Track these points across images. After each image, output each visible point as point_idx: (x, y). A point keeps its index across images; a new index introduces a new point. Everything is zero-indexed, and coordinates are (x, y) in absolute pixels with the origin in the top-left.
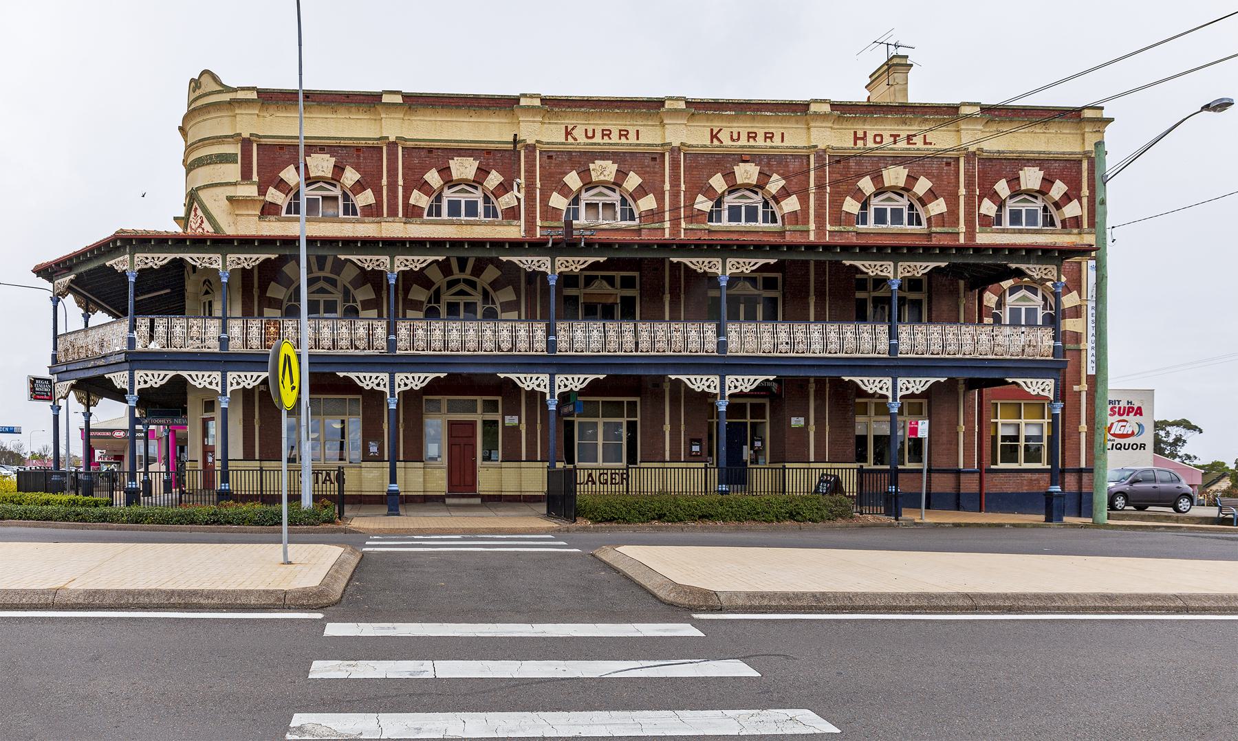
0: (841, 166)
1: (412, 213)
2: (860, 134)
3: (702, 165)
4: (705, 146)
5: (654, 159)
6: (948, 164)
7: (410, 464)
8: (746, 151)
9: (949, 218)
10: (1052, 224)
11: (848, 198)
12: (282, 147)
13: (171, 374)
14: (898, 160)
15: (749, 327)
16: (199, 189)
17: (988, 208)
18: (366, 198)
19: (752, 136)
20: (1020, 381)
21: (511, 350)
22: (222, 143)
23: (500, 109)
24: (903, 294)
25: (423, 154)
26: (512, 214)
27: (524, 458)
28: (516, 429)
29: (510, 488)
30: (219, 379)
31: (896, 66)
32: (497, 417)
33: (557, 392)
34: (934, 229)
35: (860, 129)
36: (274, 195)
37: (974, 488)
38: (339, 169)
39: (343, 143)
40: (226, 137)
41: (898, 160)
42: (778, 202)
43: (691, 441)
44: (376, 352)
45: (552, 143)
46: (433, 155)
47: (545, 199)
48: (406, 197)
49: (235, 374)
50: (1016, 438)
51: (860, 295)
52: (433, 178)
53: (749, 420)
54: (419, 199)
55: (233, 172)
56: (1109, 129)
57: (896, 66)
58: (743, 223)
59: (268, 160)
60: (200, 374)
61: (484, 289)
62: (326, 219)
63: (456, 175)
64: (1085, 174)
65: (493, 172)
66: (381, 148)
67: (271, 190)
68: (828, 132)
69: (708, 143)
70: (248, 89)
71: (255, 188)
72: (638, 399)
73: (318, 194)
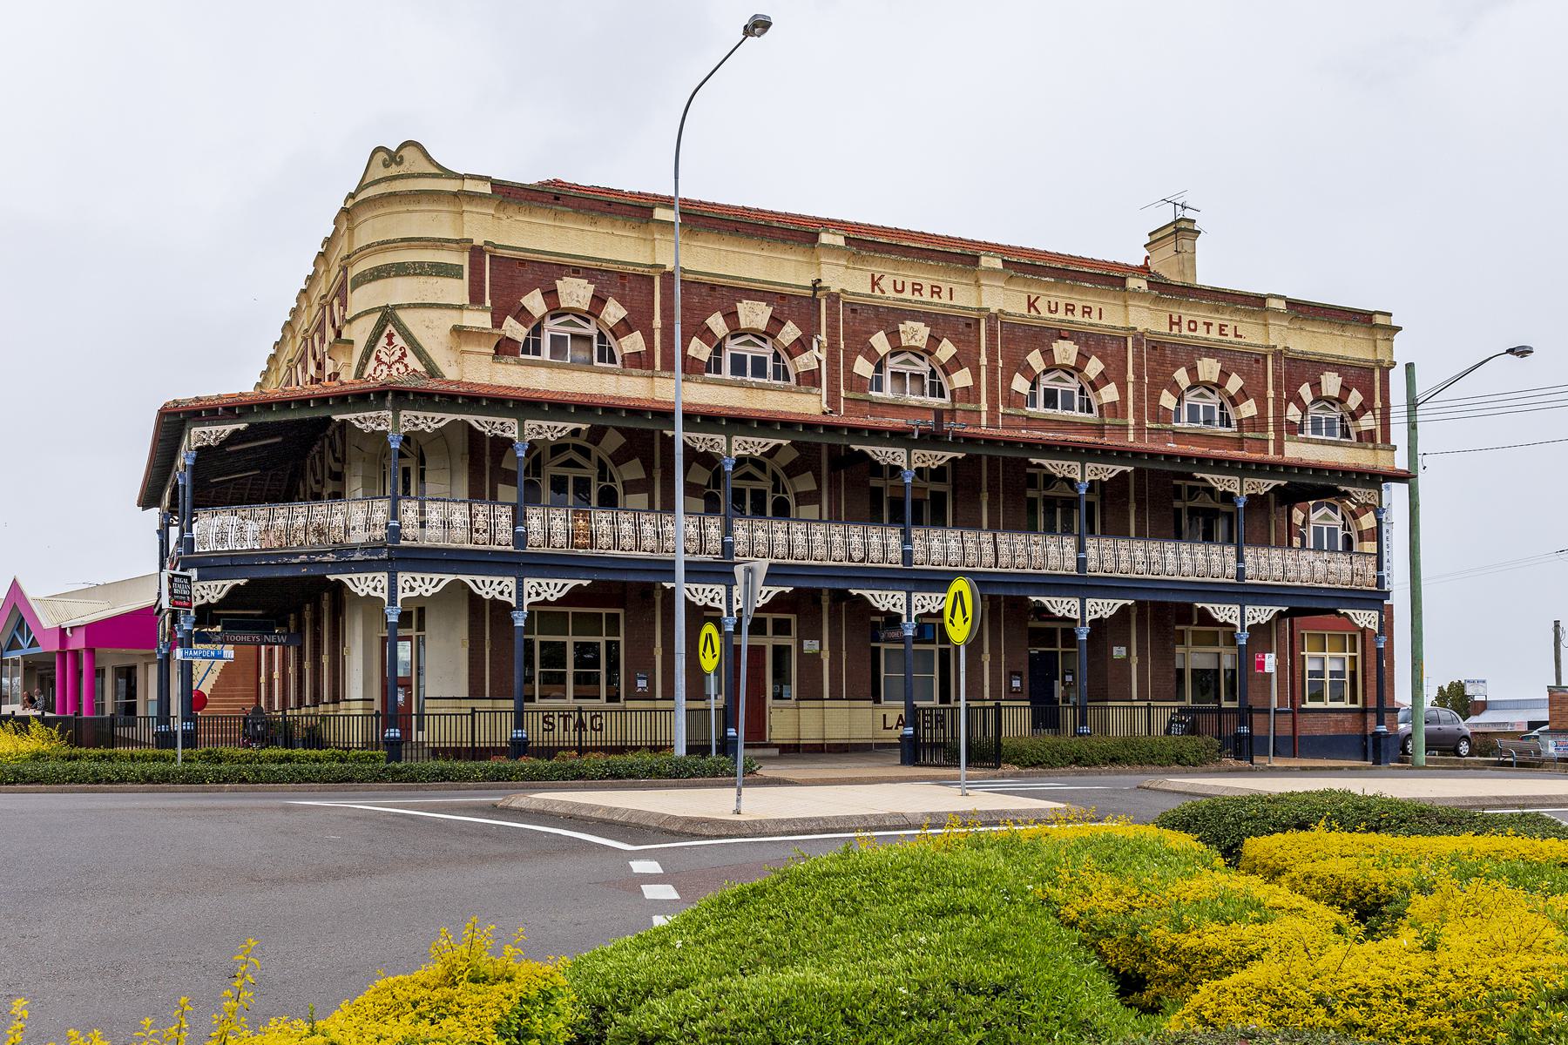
0: (1157, 353)
1: (692, 368)
2: (1175, 319)
3: (1163, 357)
4: (1022, 316)
5: (968, 325)
6: (1257, 361)
7: (803, 704)
8: (1065, 326)
9: (1258, 423)
10: (1348, 436)
11: (1165, 391)
12: (522, 262)
13: (449, 578)
14: (1211, 351)
15: (935, 533)
16: (400, 307)
17: (1293, 413)
18: (633, 342)
19: (1070, 309)
20: (1350, 612)
21: (862, 560)
22: (442, 248)
23: (799, 244)
24: (922, 484)
25: (704, 291)
26: (810, 379)
27: (826, 695)
28: (816, 657)
29: (810, 735)
30: (513, 587)
31: (1181, 231)
32: (790, 641)
33: (914, 613)
34: (1108, 421)
35: (1177, 311)
36: (515, 330)
37: (1286, 730)
38: (599, 301)
39: (605, 266)
40: (448, 241)
41: (1211, 351)
42: (947, 374)
43: (1012, 674)
44: (710, 558)
45: (858, 294)
46: (717, 294)
47: (1009, 379)
48: (685, 348)
49: (534, 581)
50: (1321, 674)
51: (1030, 493)
52: (717, 323)
53: (1060, 649)
54: (700, 350)
55: (457, 291)
56: (1397, 337)
57: (1181, 231)
58: (1059, 411)
59: (504, 279)
60: (488, 580)
61: (600, 460)
62: (576, 366)
63: (744, 323)
64: (1377, 384)
65: (789, 323)
66: (652, 279)
67: (509, 321)
68: (1146, 314)
69: (1025, 312)
70: (480, 178)
71: (488, 316)
72: (621, 611)
73: (566, 331)
